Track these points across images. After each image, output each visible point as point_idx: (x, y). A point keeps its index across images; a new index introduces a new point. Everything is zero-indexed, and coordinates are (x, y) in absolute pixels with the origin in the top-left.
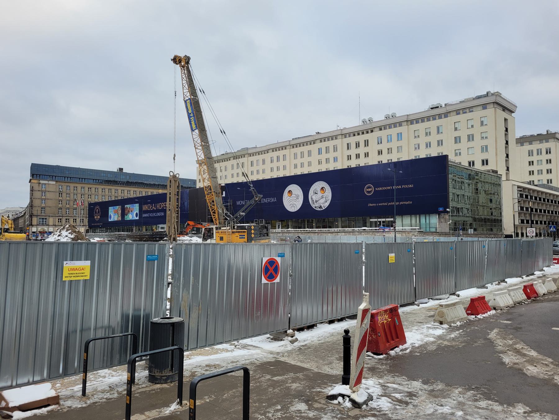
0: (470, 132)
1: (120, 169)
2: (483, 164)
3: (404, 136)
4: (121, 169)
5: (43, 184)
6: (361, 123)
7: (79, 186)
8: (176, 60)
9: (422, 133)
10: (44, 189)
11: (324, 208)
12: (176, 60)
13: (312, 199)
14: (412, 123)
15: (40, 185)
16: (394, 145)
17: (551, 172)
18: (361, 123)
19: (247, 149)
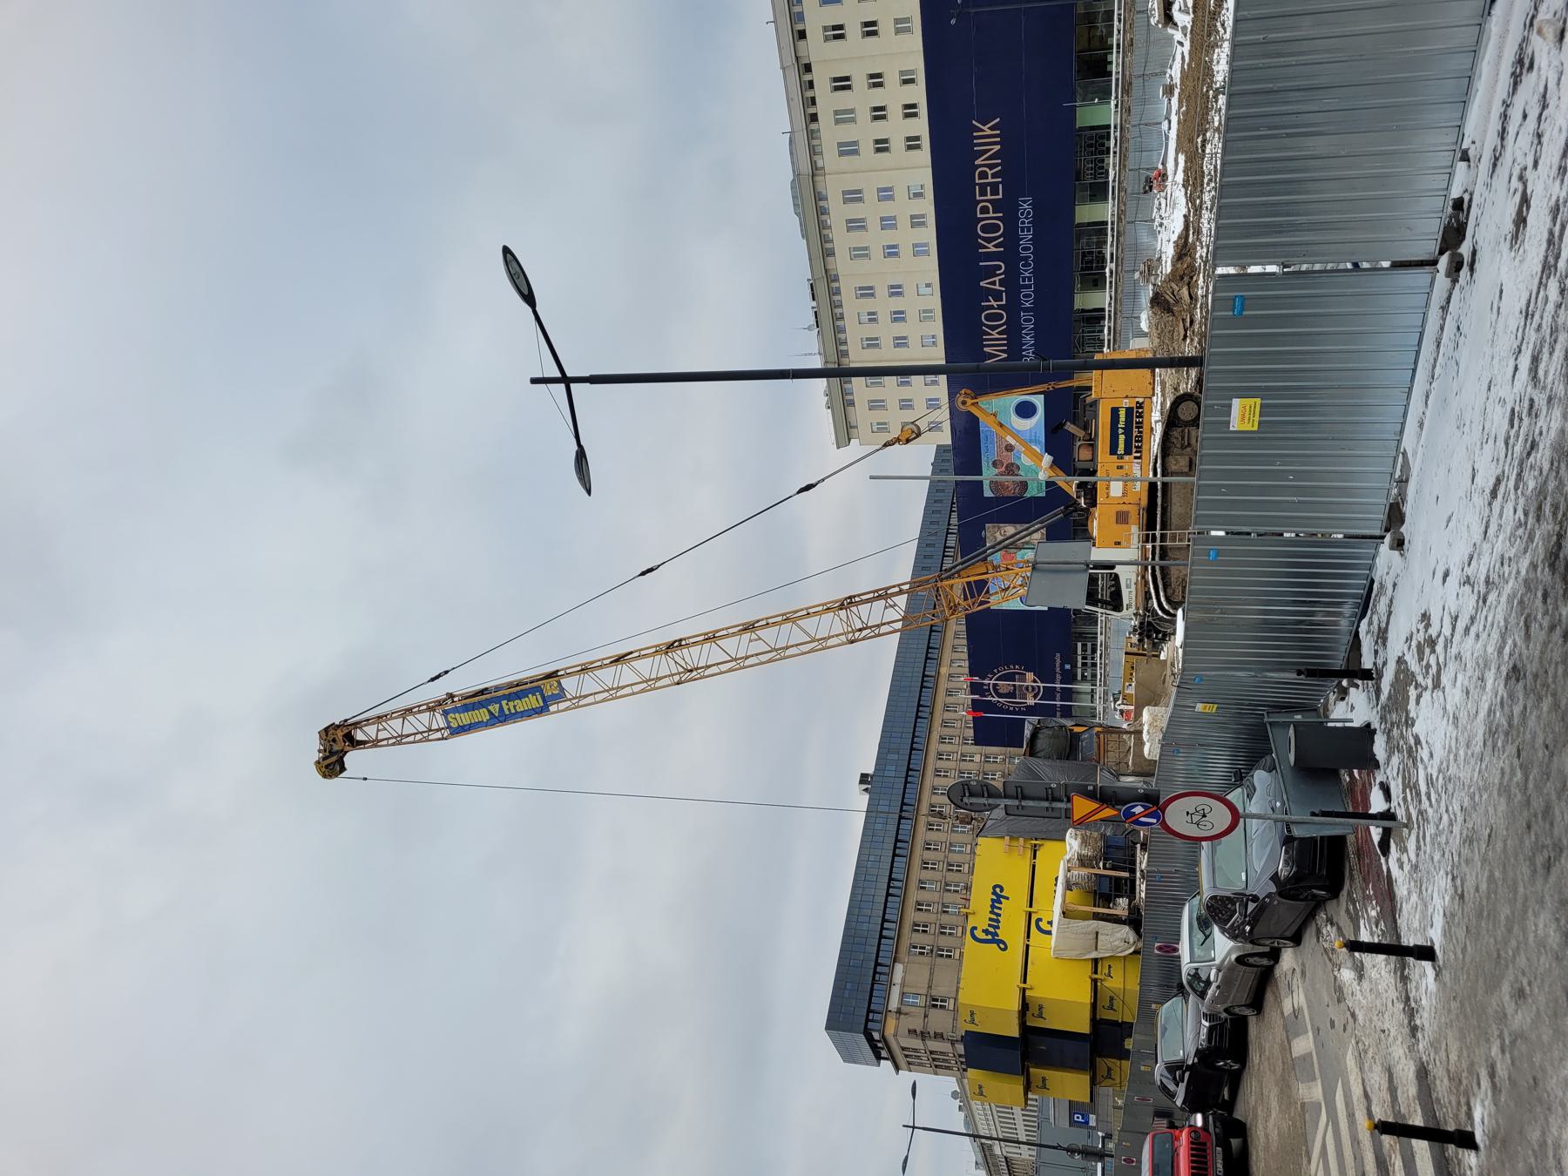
1: (861, 782)
2: (918, 147)
4: (864, 778)
5: (901, 1002)
7: (914, 895)
8: (332, 765)
10: (920, 1001)
12: (332, 765)
15: (904, 1009)
17: (879, 76)
19: (797, 175)
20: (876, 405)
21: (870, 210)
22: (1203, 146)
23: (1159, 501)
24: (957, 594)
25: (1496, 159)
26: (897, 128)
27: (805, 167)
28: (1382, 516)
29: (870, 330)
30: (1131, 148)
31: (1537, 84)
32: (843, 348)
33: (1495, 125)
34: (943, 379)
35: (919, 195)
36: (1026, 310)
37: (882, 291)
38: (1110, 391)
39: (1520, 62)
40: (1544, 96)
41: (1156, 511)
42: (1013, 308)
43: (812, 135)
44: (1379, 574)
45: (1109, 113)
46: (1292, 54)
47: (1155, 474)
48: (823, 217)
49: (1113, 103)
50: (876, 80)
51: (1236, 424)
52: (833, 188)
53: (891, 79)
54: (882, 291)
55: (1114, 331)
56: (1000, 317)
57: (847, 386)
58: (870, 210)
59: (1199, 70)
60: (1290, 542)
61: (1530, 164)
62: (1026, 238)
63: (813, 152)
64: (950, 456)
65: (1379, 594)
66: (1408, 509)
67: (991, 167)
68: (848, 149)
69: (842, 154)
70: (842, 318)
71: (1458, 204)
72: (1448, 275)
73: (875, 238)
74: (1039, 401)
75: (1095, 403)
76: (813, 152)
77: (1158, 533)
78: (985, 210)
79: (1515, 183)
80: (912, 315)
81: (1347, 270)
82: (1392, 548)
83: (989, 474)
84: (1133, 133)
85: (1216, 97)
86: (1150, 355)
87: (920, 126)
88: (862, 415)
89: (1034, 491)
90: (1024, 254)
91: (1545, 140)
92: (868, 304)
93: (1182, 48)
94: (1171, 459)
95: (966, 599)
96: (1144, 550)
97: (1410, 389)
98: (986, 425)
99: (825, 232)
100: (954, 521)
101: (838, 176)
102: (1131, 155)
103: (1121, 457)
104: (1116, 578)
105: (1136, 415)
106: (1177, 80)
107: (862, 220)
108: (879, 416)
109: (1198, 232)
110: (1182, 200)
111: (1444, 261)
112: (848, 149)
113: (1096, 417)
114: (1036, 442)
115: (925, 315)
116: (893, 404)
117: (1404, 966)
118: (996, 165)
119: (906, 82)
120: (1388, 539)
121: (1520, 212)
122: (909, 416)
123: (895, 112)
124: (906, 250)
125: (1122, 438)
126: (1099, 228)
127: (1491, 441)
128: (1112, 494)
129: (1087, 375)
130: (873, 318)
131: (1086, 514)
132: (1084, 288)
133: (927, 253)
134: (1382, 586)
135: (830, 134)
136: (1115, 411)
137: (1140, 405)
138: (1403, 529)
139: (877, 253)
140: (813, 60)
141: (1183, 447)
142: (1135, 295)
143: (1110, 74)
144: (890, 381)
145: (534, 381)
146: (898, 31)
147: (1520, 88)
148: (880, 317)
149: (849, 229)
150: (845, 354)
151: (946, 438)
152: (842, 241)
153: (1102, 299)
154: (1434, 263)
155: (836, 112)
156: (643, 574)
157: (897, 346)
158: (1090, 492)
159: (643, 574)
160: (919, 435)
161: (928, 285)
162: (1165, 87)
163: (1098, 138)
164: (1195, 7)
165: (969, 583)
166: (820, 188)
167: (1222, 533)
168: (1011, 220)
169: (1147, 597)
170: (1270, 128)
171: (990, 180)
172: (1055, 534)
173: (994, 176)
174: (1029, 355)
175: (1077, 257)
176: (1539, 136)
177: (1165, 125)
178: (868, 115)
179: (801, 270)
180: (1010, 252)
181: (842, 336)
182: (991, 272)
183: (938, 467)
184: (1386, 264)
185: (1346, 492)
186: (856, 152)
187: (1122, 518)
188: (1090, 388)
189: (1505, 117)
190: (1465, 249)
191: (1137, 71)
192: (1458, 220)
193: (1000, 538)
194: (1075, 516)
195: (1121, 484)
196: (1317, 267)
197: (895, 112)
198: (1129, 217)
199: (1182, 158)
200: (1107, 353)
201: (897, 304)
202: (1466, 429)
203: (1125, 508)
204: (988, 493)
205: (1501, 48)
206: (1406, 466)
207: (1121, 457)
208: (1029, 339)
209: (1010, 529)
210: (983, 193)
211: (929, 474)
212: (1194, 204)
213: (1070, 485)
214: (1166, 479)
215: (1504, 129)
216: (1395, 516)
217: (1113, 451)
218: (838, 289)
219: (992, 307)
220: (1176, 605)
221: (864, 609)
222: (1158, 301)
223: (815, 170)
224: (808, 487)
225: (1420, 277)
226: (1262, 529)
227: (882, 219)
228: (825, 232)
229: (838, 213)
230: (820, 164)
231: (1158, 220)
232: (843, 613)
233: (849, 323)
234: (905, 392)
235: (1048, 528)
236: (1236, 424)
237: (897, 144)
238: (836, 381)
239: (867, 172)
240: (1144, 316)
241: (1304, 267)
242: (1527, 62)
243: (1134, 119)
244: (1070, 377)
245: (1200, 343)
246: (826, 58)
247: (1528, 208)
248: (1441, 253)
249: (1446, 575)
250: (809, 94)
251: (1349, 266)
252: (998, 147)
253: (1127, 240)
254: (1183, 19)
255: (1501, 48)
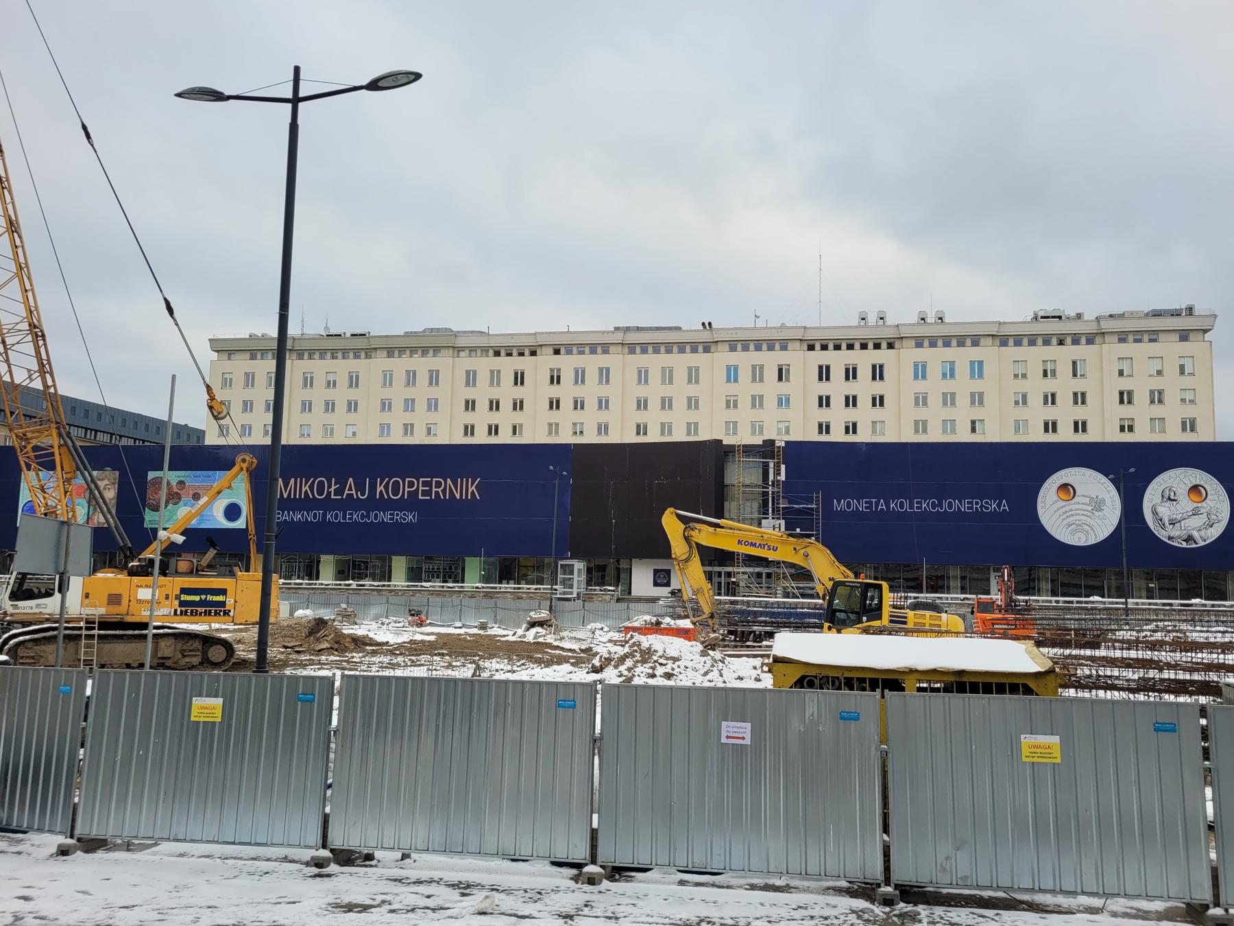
0: (1157, 384)
3: (1090, 369)
6: (855, 321)
9: (1035, 371)
11: (1202, 544)
13: (1155, 513)
14: (1004, 343)
16: (591, 391)
18: (855, 321)
19: (456, 334)
20: (249, 379)
21: (422, 392)
22: (439, 654)
23: (130, 632)
24: (44, 441)
25: (400, 881)
26: (482, 418)
27: (461, 342)
28: (95, 832)
29: (319, 381)
30: (445, 599)
31: (451, 902)
32: (306, 355)
33: (425, 875)
34: (268, 441)
35: (429, 431)
36: (324, 515)
37: (353, 394)
38: (242, 590)
39: (468, 886)
40: (442, 908)
41: (119, 628)
42: (328, 505)
43: (485, 350)
44: (33, 837)
45: (473, 582)
46: (495, 723)
47: (156, 628)
48: (420, 352)
49: (479, 585)
50: (518, 405)
51: (197, 702)
52: (442, 362)
53: (518, 417)
54: (353, 394)
55: (298, 588)
56: (320, 493)
57: (270, 355)
58: (422, 392)
59: (494, 648)
60: (73, 754)
61: (392, 907)
62: (385, 517)
63: (472, 350)
64: (193, 442)
65: (11, 840)
66: (100, 855)
67: (444, 491)
68: (471, 378)
69: (468, 372)
70: (333, 357)
71: (369, 857)
72: (313, 858)
73: (398, 393)
74: (240, 524)
75: (232, 574)
76: (472, 350)
77: (96, 632)
78: (411, 484)
79: (380, 898)
80: (330, 418)
81: (326, 779)
82: (59, 846)
83: (173, 477)
84: (456, 600)
85: (474, 662)
86: (272, 620)
87: (481, 438)
88: (241, 365)
89: (149, 517)
90: (372, 515)
91: (410, 915)
92: (343, 381)
93: (510, 635)
94: (171, 641)
95: (35, 448)
96: (79, 620)
97: (217, 842)
98: (220, 478)
99: (408, 352)
100: (124, 442)
102: (439, 599)
103: (178, 597)
104: (49, 594)
105: (219, 609)
106: (490, 632)
107: (414, 384)
108: (239, 380)
109: (374, 653)
110: (400, 640)
111: (325, 853)
112: (471, 378)
113: (219, 576)
114: (201, 521)
115: (329, 430)
116: (249, 394)
117: (61, 613)
118: (445, 495)
119: (515, 428)
120: (70, 841)
121: (357, 905)
122: (236, 410)
123: (494, 418)
124: (386, 418)
125: (197, 598)
126: (386, 575)
127: (160, 917)
128: (140, 590)
129: (260, 568)
130: (331, 384)
131: (122, 567)
132: (338, 562)
133: (381, 435)
134: (20, 841)
135: (484, 365)
136: (223, 592)
137: (226, 613)
138: (79, 853)
139: (387, 393)
140: (538, 358)
141: (182, 651)
142: (327, 604)
143: (500, 582)
144: (270, 394)
145: (297, 70)
146: (550, 425)
147: (450, 889)
148: (331, 391)
149: (408, 372)
150: (301, 357)
151: (212, 439)
152: (400, 365)
153: (327, 578)
154: (324, 847)
155: (499, 372)
156: (84, 128)
157: (304, 403)
158: (145, 570)
159: (84, 128)
160: (216, 418)
161: (354, 434)
162: (486, 623)
163: (454, 573)
164: (538, 643)
165: (52, 454)
166: (443, 352)
167: (88, 692)
168: (401, 505)
169: (24, 624)
170: (445, 712)
171: (434, 490)
172: (101, 537)
173: (437, 493)
175: (363, 557)
176: (413, 910)
177: (458, 624)
178: (494, 397)
179: (728, 320)
180: (374, 504)
181: (340, 355)
182: (360, 487)
183: (180, 430)
184: (328, 810)
185: (122, 800)
186: (468, 384)
187: (114, 599)
188: (248, 570)
189: (431, 881)
190: (333, 868)
191: (500, 603)
192: (357, 858)
193: (101, 484)
194: (120, 557)
195: (151, 599)
196: (332, 756)
197: (494, 418)
198: (392, 599)
199: (432, 638)
200: (277, 581)
201: (341, 406)
202: (174, 894)
203: (125, 602)
204: (151, 475)
205: (480, 870)
206: (144, 847)
207: (178, 597)
208: (298, 517)
209: (110, 494)
210: (424, 484)
211: (174, 421)
212: (396, 649)
213: (153, 553)
214: (150, 638)
215: (421, 882)
216: (92, 845)
217: (184, 591)
218: (337, 358)
219: (330, 487)
220: (13, 652)
221: (30, 347)
222: (320, 623)
223: (458, 350)
224: (170, 310)
225: (314, 836)
226: (89, 732)
228: (408, 352)
229: (422, 364)
230: (462, 354)
231: (387, 621)
232: (25, 326)
233: (328, 364)
234: (259, 407)
235: (108, 529)
236: (197, 702)
237: (470, 418)
238: (275, 345)
239: (452, 391)
240: (308, 612)
241: (333, 746)
242: (467, 891)
243: (466, 601)
244: (259, 551)
245: (280, 660)
246: (538, 368)
247: (359, 912)
248: (332, 851)
249: (26, 898)
250: (515, 352)
251: (329, 781)
252: (458, 497)
253: (374, 597)
254: (530, 636)
255: (480, 870)
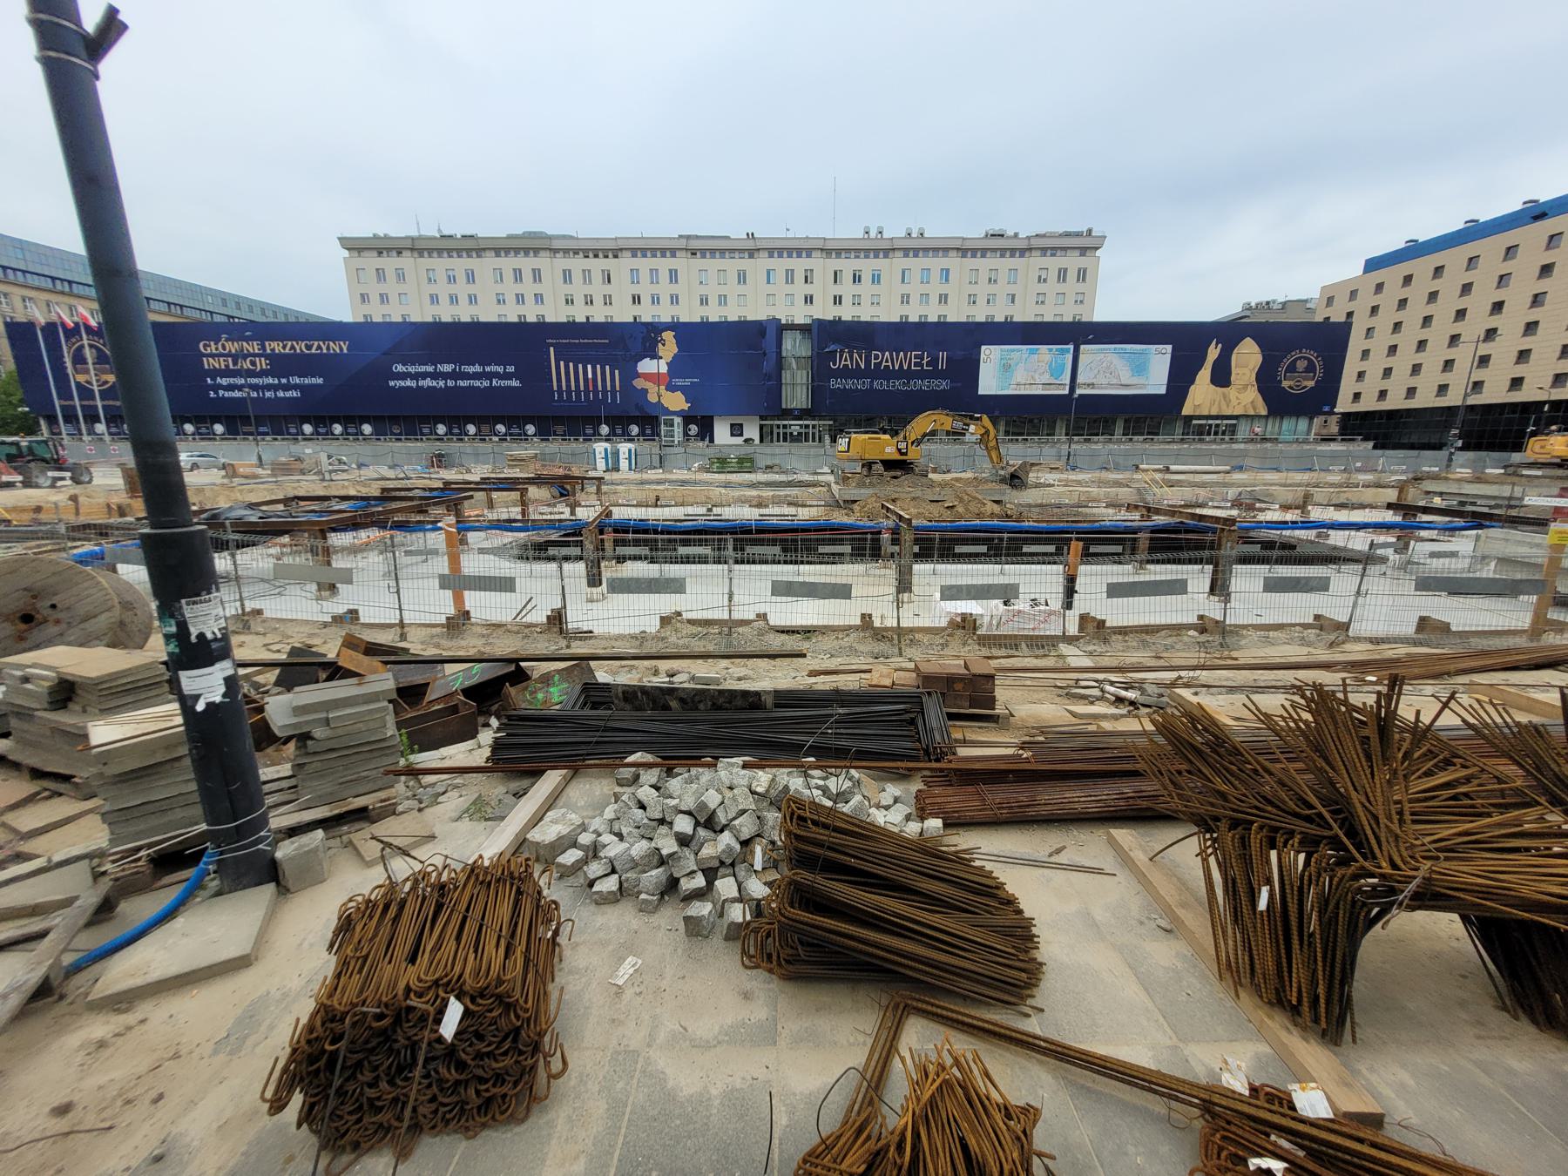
19: (550, 238)
27: (556, 244)
52: (543, 262)
68: (567, 276)
76: (566, 251)
101: (550, 266)
130: (452, 279)
152: (508, 263)
166: (542, 253)
174: (835, 384)
227: (948, 270)
229: (526, 263)
239: (552, 286)
